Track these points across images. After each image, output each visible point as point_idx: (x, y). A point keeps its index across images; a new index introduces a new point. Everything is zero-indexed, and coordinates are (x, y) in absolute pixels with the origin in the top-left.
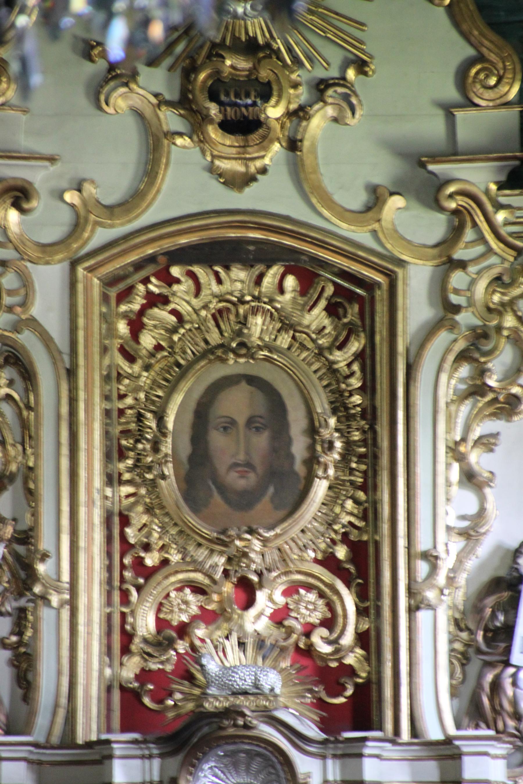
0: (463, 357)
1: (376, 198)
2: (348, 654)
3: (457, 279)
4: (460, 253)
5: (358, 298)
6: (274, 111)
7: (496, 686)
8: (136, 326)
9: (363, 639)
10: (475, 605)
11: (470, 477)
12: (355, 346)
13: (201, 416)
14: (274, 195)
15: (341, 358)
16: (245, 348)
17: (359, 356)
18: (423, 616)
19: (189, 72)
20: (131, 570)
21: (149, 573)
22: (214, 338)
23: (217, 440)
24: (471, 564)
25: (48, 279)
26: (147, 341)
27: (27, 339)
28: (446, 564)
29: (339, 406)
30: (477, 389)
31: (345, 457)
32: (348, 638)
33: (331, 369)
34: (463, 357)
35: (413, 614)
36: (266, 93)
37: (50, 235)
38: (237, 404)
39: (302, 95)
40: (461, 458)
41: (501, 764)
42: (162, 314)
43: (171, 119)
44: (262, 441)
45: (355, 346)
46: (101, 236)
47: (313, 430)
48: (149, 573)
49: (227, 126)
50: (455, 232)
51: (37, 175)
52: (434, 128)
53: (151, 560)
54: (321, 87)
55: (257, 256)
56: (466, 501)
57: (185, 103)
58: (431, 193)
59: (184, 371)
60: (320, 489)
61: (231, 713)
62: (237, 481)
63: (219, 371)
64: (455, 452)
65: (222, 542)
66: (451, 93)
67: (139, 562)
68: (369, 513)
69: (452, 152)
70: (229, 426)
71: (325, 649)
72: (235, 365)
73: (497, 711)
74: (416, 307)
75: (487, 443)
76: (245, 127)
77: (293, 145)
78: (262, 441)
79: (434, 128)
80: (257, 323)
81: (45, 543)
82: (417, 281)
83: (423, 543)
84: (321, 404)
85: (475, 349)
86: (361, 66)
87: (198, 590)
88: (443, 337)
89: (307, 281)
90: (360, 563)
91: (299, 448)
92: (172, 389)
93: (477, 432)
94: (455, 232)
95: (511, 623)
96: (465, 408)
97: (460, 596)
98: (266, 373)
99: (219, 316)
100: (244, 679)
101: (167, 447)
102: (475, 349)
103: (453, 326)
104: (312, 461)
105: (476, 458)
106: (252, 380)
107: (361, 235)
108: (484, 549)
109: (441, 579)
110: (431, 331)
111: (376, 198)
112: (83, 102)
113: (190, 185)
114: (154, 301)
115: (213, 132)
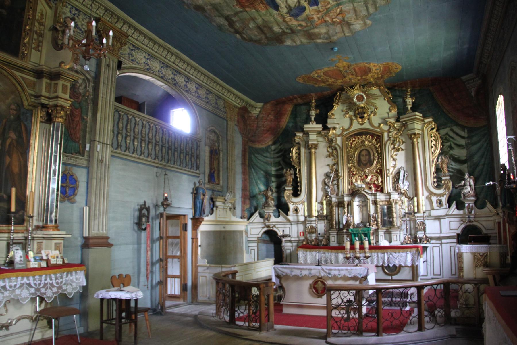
0: (392, 144)
1: (380, 124)
2: (74, 178)
3: (390, 134)
4: (391, 131)
5: (379, 137)
6: (366, 115)
7: (398, 186)
8: (351, 144)
9: (382, 181)
10: (395, 176)
11: (394, 160)
12: (379, 144)
13: (360, 155)
14: (367, 126)
15: (377, 146)
16: (364, 145)
17: (380, 145)
18: (388, 178)
19: (355, 111)
20: (351, 175)
21: (354, 175)
22: (361, 145)
23: (362, 157)
24: (394, 171)
25: (339, 139)
26: (353, 146)
27: (337, 146)
28: (391, 171)
29: (377, 152)
30: (394, 148)
31: (378, 158)
32: (380, 182)
33: (376, 148)
34: (392, 144)
35: (365, 216)
36: (365, 113)
37: (339, 133)
38: (364, 153)
39: (370, 113)
40: (393, 157)
41: (315, 136)
42: (355, 142)
43: (354, 118)
44: (367, 157)
45: (379, 144)
46: (345, 133)
47: (374, 155)
48: (354, 175)
49: (360, 118)
50: (390, 128)
51: (337, 126)
52: (386, 115)
53: (354, 173)
54: (371, 112)
55: (366, 134)
56: (394, 163)
57: (355, 116)
58: (386, 123)
59: (357, 149)
60: (375, 163)
61: (358, 190)
62: (365, 162)
63: (362, 149)
64: (392, 156)
65: (363, 170)
66: (388, 111)
67: (353, 174)
68: (382, 166)
69: (389, 118)
70: (363, 155)
71: (377, 183)
72: (363, 148)
73: (398, 189)
74: (386, 138)
75: (396, 155)
76: (362, 118)
77: (368, 119)
78: (367, 157)
79: (386, 115)
80: (366, 143)
81: (340, 171)
82: (386, 134)
83: (388, 168)
84: (375, 152)
85: (393, 143)
86: (376, 109)
87: (361, 176)
88: (389, 142)
89: (373, 137)
90: (380, 172)
91: (372, 158)
92: (355, 151)
93: (395, 153)
94: (390, 128)
95: (194, 231)
96: (393, 151)
97: (393, 175)
98: (367, 148)
99: (361, 142)
100: (360, 186)
101: (355, 159)
102: (393, 143)
103: (390, 140)
104: (374, 159)
105: (394, 157)
106: (366, 150)
107: (378, 130)
108: (396, 169)
109: (390, 173)
110: (387, 141)
111: (380, 124)
112: (342, 117)
113: (356, 126)
114: (354, 141)
115: (358, 118)
